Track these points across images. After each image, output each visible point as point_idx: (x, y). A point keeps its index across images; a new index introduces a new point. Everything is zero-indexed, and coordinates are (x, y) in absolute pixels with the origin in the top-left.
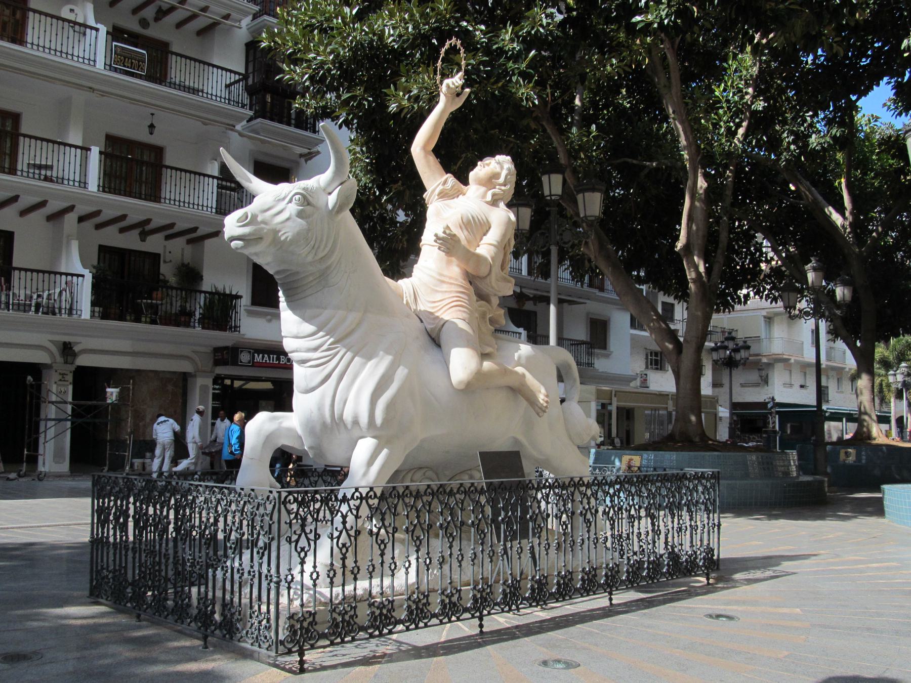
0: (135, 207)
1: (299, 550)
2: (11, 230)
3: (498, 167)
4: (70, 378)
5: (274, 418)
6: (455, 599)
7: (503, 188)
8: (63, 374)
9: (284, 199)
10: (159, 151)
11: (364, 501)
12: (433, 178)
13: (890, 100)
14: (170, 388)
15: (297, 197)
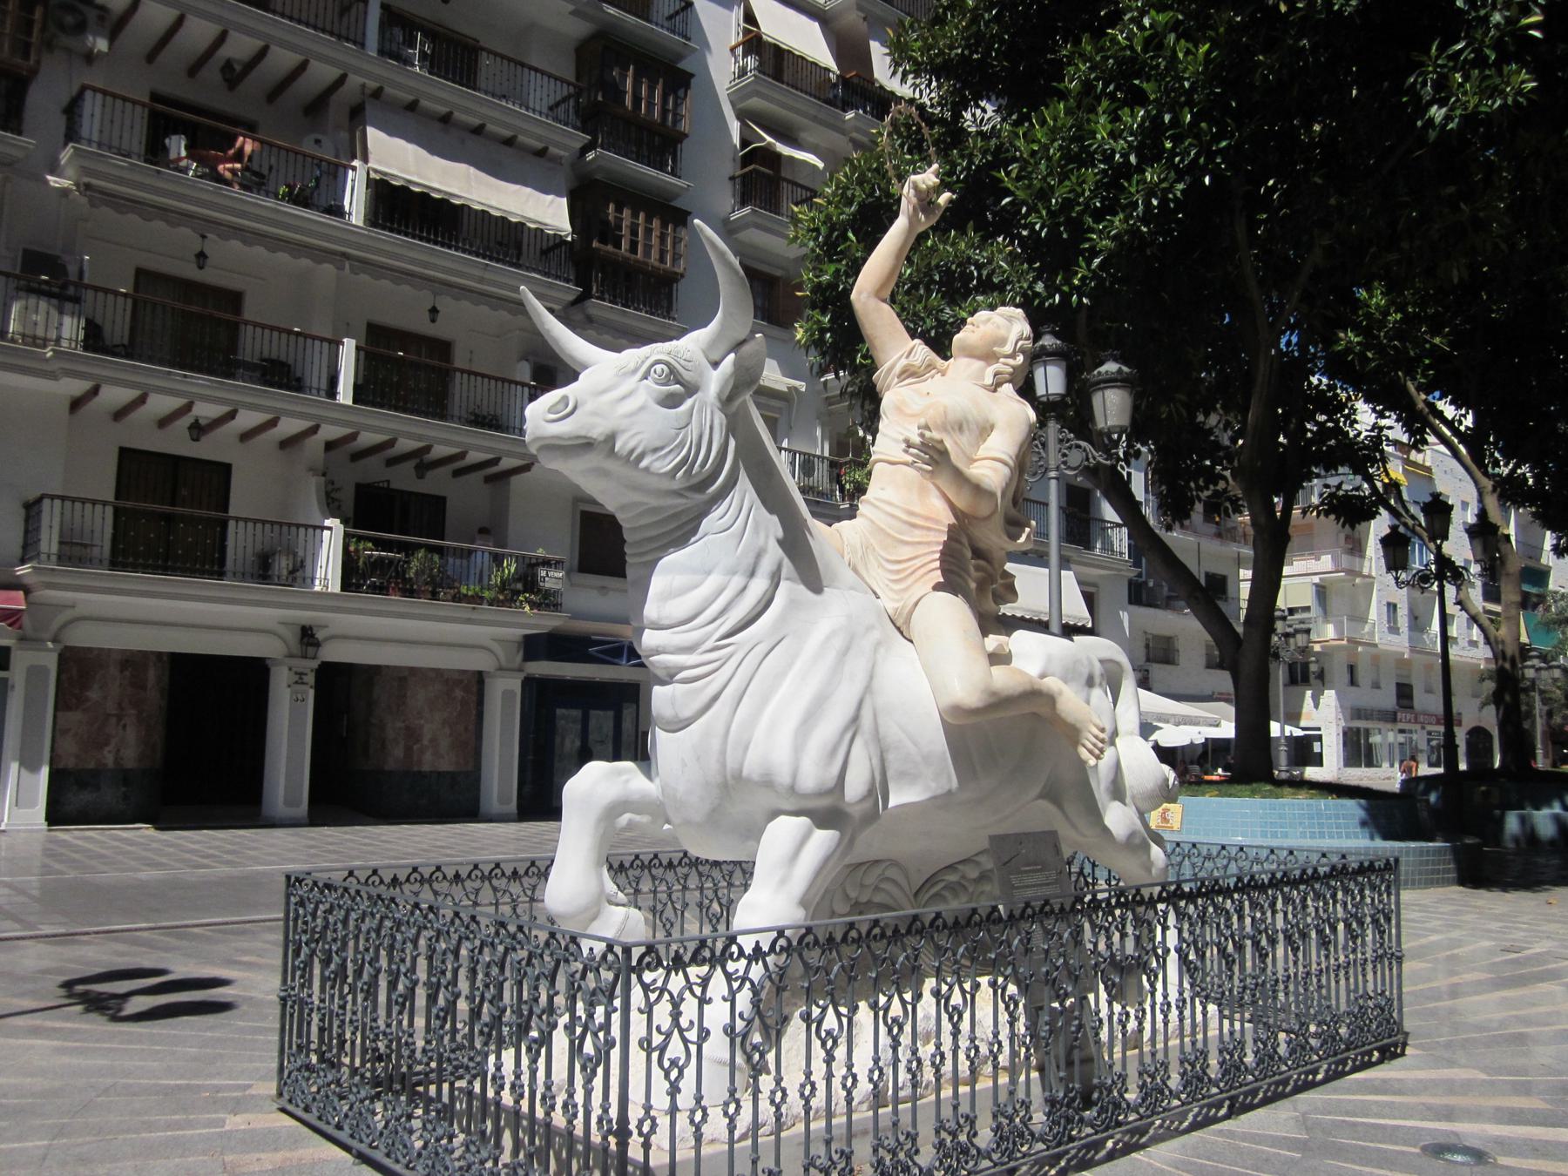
0: (408, 430)
1: (666, 1064)
2: (227, 460)
3: (1000, 327)
4: (311, 679)
5: (620, 773)
6: (963, 1138)
7: (1011, 361)
8: (301, 674)
9: (635, 371)
10: (443, 348)
11: (795, 955)
12: (894, 345)
13: (1061, 432)
14: (459, 693)
15: (659, 367)
